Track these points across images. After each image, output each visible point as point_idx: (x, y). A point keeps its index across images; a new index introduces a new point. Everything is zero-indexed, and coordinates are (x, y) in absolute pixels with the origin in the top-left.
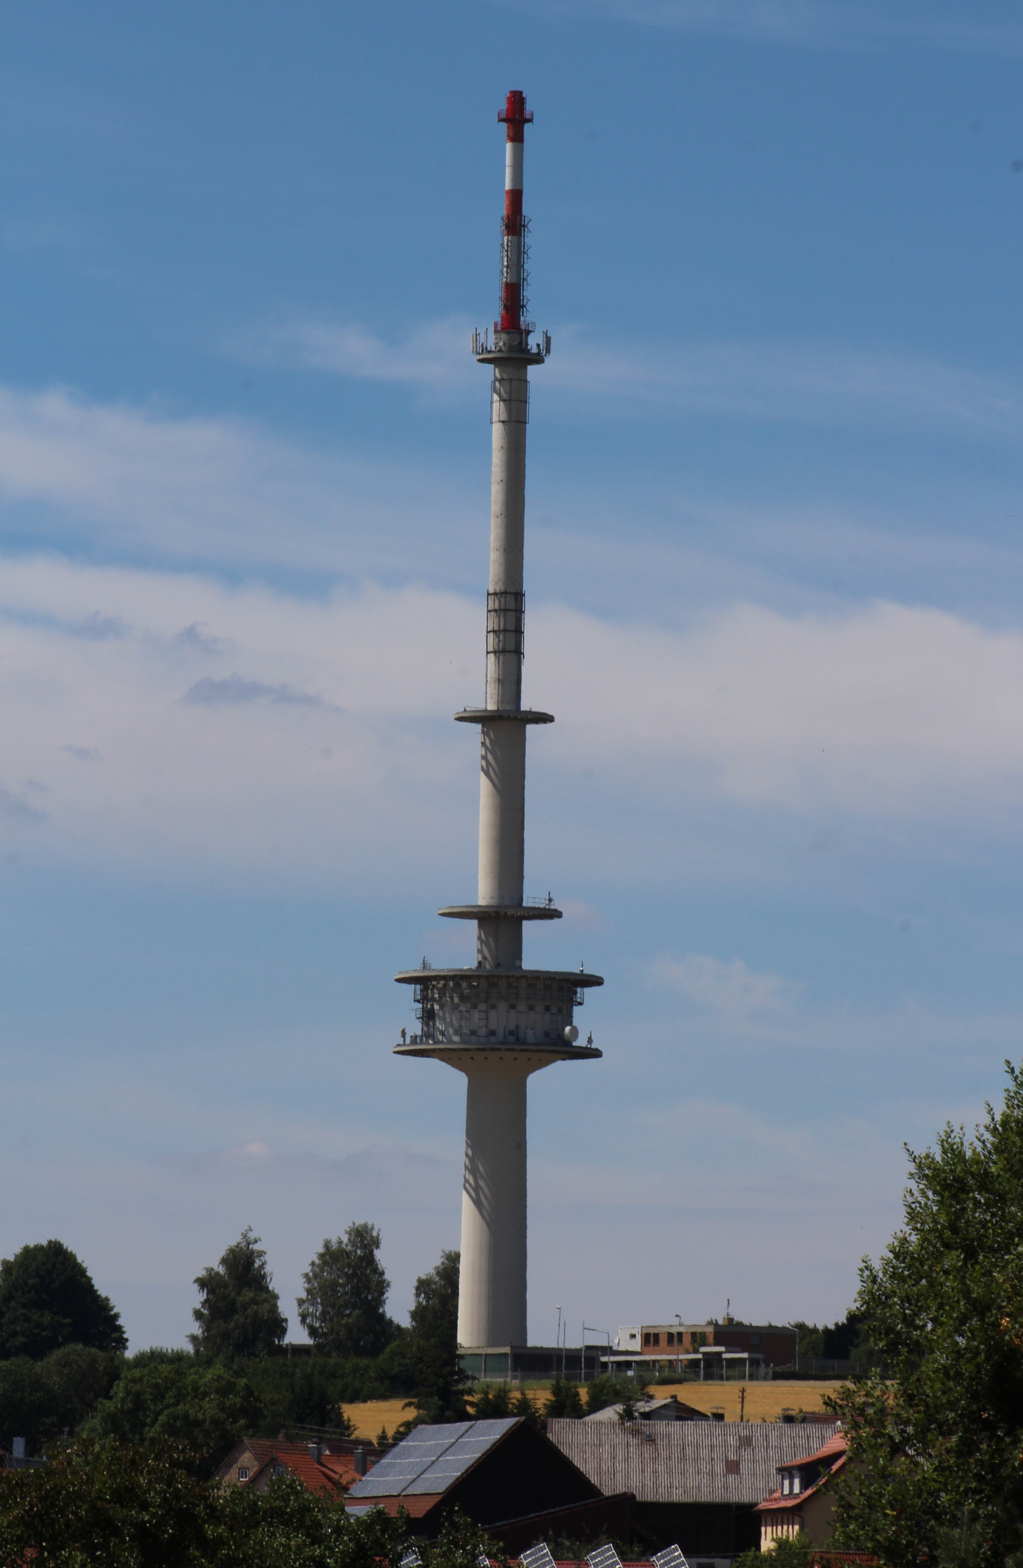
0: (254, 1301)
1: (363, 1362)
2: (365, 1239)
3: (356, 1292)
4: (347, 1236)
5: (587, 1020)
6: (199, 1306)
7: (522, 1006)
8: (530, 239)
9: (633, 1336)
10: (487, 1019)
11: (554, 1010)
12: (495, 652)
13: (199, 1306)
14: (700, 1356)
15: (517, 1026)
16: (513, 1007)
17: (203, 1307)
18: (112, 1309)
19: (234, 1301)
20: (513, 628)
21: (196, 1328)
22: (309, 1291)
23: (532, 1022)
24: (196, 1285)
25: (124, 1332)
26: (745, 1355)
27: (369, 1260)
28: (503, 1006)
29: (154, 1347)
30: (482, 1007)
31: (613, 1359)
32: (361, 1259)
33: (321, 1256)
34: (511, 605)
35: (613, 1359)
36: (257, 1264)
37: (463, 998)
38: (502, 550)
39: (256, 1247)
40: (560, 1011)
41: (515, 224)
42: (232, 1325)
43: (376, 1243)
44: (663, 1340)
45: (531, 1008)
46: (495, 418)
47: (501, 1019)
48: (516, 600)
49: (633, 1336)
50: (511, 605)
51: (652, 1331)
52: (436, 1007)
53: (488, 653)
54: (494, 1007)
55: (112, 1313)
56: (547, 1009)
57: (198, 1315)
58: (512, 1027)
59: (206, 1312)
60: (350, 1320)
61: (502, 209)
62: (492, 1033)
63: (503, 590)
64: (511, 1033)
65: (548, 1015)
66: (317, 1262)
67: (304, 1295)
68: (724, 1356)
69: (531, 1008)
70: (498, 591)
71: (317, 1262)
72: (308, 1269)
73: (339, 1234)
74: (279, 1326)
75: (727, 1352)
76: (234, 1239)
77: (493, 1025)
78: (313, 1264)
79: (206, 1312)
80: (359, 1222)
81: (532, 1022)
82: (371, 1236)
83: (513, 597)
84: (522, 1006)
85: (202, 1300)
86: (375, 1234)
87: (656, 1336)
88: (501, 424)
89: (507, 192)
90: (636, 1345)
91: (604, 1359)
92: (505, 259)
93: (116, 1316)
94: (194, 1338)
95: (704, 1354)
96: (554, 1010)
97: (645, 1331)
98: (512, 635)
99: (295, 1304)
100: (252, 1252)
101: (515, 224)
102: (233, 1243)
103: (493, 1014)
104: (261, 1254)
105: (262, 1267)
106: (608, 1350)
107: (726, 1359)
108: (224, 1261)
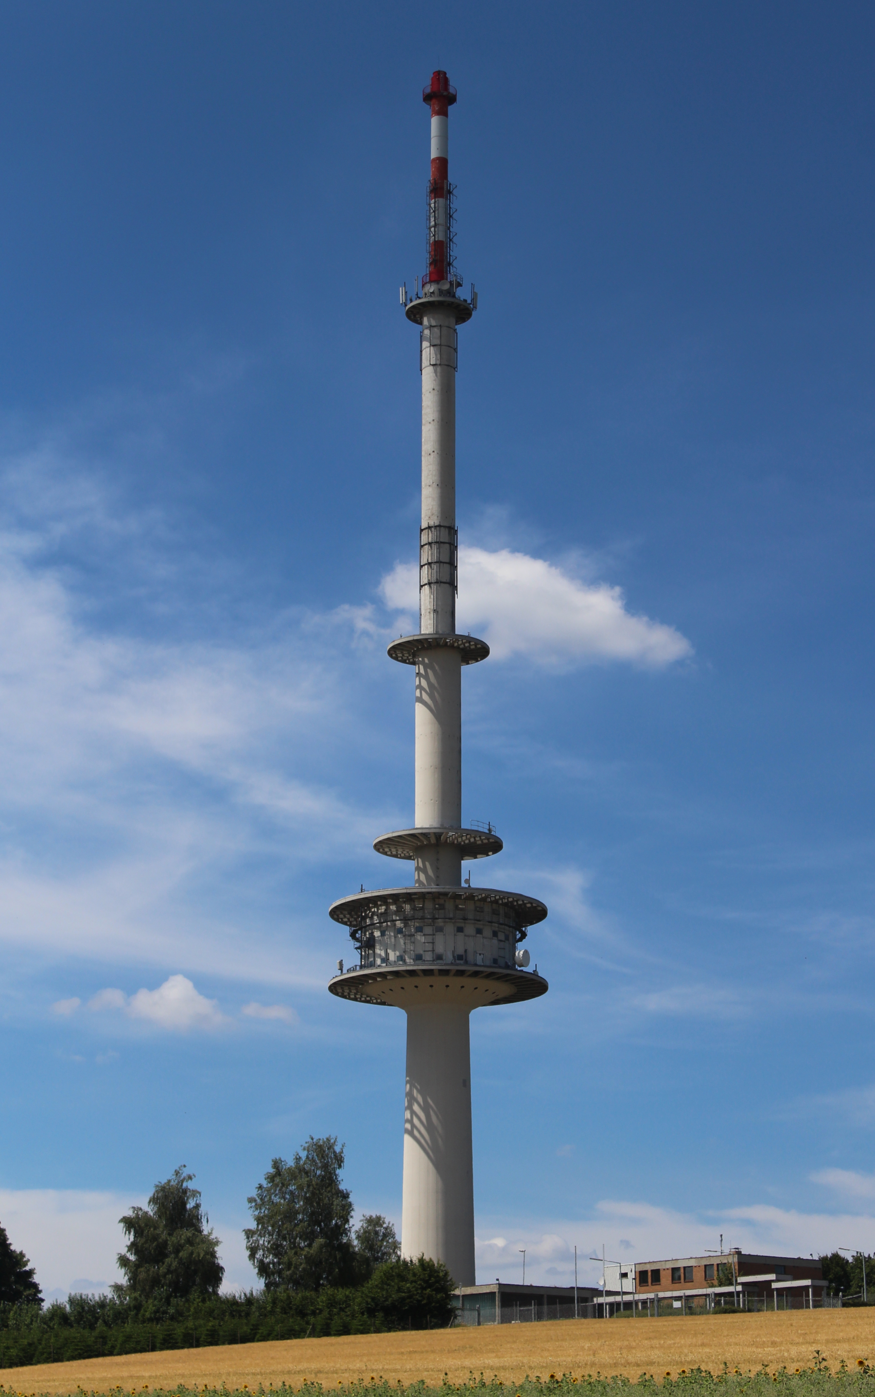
0: (189, 1241)
1: (341, 1293)
2: (325, 1159)
3: (314, 1219)
4: (306, 1152)
5: (536, 948)
6: (124, 1251)
7: (470, 929)
8: (457, 202)
9: (624, 1275)
10: (433, 943)
11: (501, 936)
12: (429, 584)
13: (124, 1251)
14: (739, 1288)
15: (466, 951)
16: (460, 930)
17: (129, 1251)
18: (25, 1264)
19: (165, 1242)
20: (447, 560)
21: (121, 1277)
22: (259, 1220)
23: (481, 948)
24: (122, 1225)
25: (40, 1292)
26: (807, 1282)
27: (329, 1181)
28: (450, 928)
29: (73, 1294)
30: (428, 930)
31: (611, 1299)
32: (323, 1178)
33: (271, 1178)
34: (445, 538)
35: (611, 1299)
36: (190, 1205)
37: (405, 920)
38: (435, 485)
39: (190, 1185)
40: (507, 938)
41: (440, 188)
42: (163, 1270)
43: (339, 1160)
44: (666, 1278)
45: (479, 931)
46: (425, 363)
47: (447, 944)
48: (450, 533)
49: (624, 1275)
50: (445, 538)
51: (649, 1268)
52: (377, 934)
53: (421, 586)
54: (440, 930)
55: (27, 1268)
56: (495, 934)
57: (123, 1261)
58: (460, 951)
59: (132, 1258)
60: (312, 1252)
61: (429, 174)
62: (439, 957)
63: (437, 523)
64: (460, 957)
65: (495, 941)
66: (265, 1184)
67: (253, 1225)
68: (774, 1285)
69: (479, 931)
70: (432, 524)
71: (265, 1184)
72: (254, 1193)
73: (291, 1151)
74: (214, 1273)
75: (777, 1280)
76: (165, 1176)
77: (440, 949)
78: (260, 1187)
79: (132, 1258)
80: (321, 1135)
81: (481, 948)
82: (335, 1152)
83: (447, 530)
84: (470, 929)
85: (129, 1243)
86: (337, 1149)
87: (656, 1274)
88: (431, 367)
89: (434, 160)
90: (629, 1285)
91: (601, 1300)
92: (432, 219)
93: (30, 1273)
94: (118, 1288)
95: (743, 1284)
96: (501, 936)
97: (641, 1268)
98: (447, 566)
99: (243, 1236)
100: (185, 1191)
101: (440, 188)
102: (164, 1181)
103: (439, 938)
104: (195, 1193)
105: (197, 1206)
106: (597, 1293)
107: (777, 1289)
108: (153, 1200)
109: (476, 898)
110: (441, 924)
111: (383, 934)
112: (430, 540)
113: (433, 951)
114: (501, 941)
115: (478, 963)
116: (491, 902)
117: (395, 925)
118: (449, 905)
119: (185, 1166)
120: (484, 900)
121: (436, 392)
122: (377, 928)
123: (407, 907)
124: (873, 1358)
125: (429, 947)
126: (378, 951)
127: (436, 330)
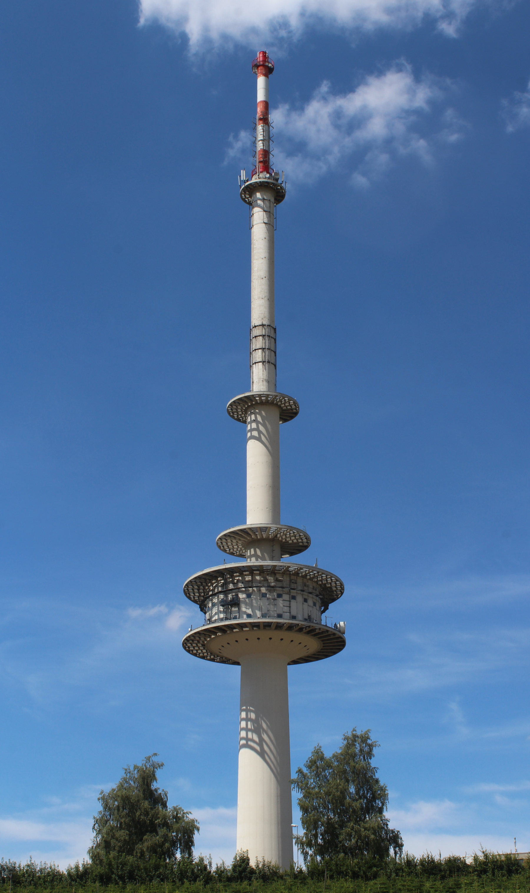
10: (290, 607)
52: (242, 596)
54: (294, 598)
62: (294, 618)
70: (264, 323)
77: (294, 613)
81: (300, 609)
88: (264, 224)
96: (310, 602)
109: (300, 575)
110: (295, 594)
111: (249, 596)
112: (264, 334)
113: (290, 613)
114: (310, 606)
115: (328, 625)
116: (302, 576)
117: (260, 590)
118: (300, 581)
119: (155, 754)
120: (297, 574)
121: (266, 240)
122: (242, 592)
123: (271, 579)
124: (75, 892)
125: (286, 609)
126: (244, 609)
127: (267, 203)
